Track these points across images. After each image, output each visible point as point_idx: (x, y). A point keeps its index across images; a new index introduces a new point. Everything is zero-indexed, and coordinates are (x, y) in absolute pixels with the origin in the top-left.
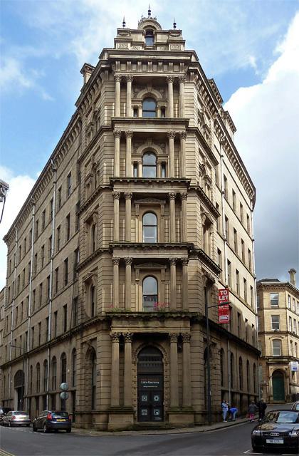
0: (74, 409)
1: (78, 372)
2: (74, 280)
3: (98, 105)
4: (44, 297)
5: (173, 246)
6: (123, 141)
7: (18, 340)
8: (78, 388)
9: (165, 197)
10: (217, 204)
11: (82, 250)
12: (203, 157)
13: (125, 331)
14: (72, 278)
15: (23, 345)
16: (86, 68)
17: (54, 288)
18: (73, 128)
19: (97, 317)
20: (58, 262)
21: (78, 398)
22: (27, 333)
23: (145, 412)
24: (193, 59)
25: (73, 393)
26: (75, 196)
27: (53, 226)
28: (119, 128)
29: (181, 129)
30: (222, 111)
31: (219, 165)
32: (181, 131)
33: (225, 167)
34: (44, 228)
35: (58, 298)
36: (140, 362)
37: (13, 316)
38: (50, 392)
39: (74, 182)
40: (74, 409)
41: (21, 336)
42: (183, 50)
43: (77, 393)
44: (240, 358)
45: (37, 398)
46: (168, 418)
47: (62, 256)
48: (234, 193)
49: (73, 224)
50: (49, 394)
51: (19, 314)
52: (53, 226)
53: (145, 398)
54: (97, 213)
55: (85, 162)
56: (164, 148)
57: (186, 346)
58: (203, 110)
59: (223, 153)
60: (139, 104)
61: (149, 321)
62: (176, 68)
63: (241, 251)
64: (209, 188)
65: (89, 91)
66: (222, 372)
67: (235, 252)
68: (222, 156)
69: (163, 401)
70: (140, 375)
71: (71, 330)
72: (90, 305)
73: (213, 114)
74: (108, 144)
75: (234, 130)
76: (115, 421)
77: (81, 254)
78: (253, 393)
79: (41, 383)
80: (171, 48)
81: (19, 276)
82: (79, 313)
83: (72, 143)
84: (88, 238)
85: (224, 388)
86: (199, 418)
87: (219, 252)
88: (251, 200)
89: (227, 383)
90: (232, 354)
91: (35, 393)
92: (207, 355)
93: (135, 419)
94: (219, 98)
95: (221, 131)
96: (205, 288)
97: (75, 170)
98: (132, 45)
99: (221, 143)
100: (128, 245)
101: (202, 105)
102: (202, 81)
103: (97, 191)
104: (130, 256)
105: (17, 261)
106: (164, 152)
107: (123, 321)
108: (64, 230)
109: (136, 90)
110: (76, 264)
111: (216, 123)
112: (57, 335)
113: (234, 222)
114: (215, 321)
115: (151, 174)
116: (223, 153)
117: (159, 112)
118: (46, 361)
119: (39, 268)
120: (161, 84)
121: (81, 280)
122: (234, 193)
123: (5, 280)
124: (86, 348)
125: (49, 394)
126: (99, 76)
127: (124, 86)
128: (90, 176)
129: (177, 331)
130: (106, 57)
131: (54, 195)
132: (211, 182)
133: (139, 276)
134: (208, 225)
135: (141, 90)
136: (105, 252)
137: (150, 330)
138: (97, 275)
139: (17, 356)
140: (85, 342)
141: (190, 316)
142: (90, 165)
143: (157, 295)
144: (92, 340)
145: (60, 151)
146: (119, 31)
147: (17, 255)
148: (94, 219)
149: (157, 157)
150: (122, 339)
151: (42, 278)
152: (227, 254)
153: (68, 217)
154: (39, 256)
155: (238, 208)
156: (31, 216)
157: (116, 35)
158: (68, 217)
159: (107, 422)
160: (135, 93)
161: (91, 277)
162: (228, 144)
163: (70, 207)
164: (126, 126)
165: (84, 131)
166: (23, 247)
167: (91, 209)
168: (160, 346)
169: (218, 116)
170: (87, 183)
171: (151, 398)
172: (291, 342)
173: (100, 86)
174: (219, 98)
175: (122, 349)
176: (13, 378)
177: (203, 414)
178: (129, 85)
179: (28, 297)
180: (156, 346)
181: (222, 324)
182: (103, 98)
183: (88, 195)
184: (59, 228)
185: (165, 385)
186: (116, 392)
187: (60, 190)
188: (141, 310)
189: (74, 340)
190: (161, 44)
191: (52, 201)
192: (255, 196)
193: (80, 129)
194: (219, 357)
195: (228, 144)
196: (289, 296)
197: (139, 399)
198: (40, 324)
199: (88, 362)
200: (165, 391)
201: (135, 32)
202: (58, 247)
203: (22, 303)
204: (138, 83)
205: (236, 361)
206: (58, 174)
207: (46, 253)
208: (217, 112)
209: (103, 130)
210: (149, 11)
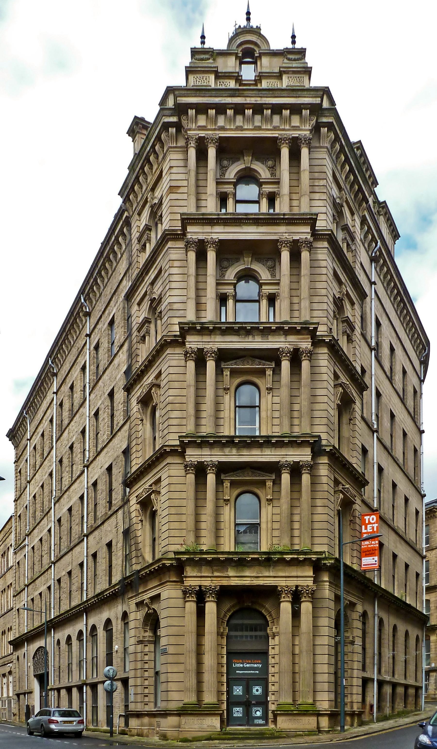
0: (127, 706)
1: (131, 649)
3: (158, 193)
4: (76, 529)
5: (286, 440)
6: (201, 258)
8: (131, 674)
9: (273, 356)
10: (362, 367)
11: (134, 450)
12: (340, 283)
13: (206, 583)
16: (137, 126)
18: (117, 239)
19: (160, 560)
20: (97, 471)
21: (131, 690)
22: (49, 588)
24: (326, 104)
25: (125, 682)
26: (123, 357)
28: (195, 232)
29: (303, 232)
31: (368, 299)
32: (303, 237)
33: (377, 303)
36: (233, 633)
38: (88, 682)
39: (119, 334)
40: (127, 706)
41: (40, 594)
42: (307, 86)
43: (131, 682)
45: (69, 690)
47: (104, 461)
48: (392, 350)
49: (119, 408)
50: (87, 685)
53: (238, 690)
54: (159, 386)
56: (272, 269)
57: (306, 607)
58: (340, 198)
61: (245, 566)
62: (296, 121)
64: (350, 340)
65: (142, 168)
66: (364, 649)
68: (374, 283)
71: (124, 579)
72: (148, 541)
73: (360, 205)
74: (176, 264)
75: (396, 236)
79: (75, 667)
80: (286, 82)
81: (34, 497)
83: (115, 264)
85: (366, 675)
86: (325, 722)
88: (421, 363)
90: (381, 622)
91: (65, 683)
96: (339, 511)
99: (373, 260)
101: (340, 188)
102: (341, 146)
104: (215, 459)
105: (29, 472)
106: (273, 275)
107: (203, 568)
108: (104, 416)
109: (225, 163)
111: (364, 221)
112: (98, 591)
113: (391, 401)
114: (355, 567)
115: (246, 314)
117: (264, 202)
118: (81, 633)
119: (66, 482)
120: (266, 149)
121: (133, 500)
122: (392, 350)
125: (87, 685)
126: (159, 138)
127: (202, 156)
128: (147, 321)
129: (292, 583)
130: (170, 103)
132: (352, 329)
134: (345, 404)
135: (233, 163)
136: (173, 452)
137: (247, 582)
138: (159, 493)
139: (37, 624)
142: (146, 304)
145: (95, 280)
146: (194, 52)
148: (154, 396)
149: (261, 285)
150: (200, 596)
153: (111, 395)
155: (398, 377)
158: (111, 395)
160: (222, 168)
163: (116, 377)
164: (208, 229)
165: (135, 241)
166: (38, 447)
167: (149, 379)
168: (264, 607)
169: (369, 209)
171: (248, 690)
173: (160, 158)
178: (212, 152)
179: (49, 531)
180: (258, 608)
183: (144, 352)
184: (96, 414)
190: (269, 76)
193: (128, 237)
194: (359, 625)
195: (385, 261)
197: (229, 692)
198: (70, 573)
199: (147, 634)
201: (222, 54)
203: (41, 540)
204: (229, 149)
205: (388, 630)
206: (94, 320)
207: (78, 458)
208: (367, 202)
209: (169, 236)
210: (248, 13)
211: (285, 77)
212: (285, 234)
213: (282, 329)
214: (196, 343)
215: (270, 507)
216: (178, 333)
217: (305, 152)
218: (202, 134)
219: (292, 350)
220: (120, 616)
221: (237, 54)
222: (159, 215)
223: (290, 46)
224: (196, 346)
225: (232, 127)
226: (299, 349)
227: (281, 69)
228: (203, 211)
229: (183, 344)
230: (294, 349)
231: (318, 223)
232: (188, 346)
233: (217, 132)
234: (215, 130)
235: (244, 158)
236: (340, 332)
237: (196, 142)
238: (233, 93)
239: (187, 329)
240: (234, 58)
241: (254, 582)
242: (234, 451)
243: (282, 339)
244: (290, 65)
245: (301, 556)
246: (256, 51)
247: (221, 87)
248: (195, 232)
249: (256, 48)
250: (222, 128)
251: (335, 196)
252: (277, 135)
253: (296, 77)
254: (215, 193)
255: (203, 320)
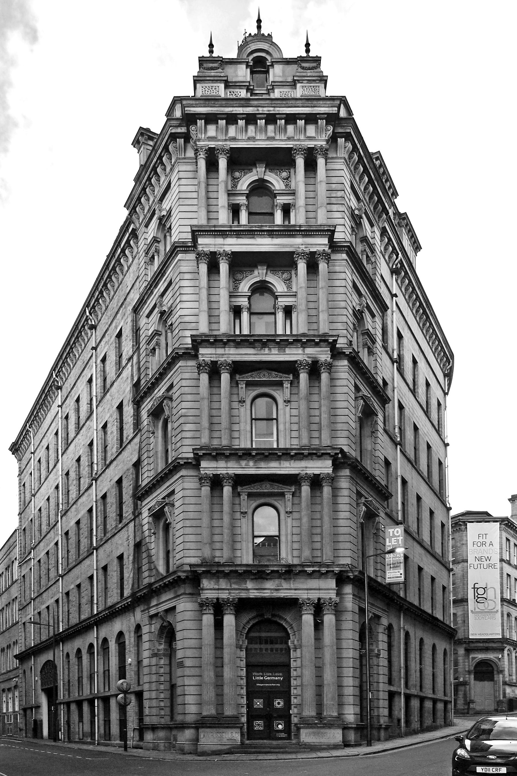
1: (146, 662)
2: (134, 513)
3: (166, 205)
4: (84, 542)
7: (44, 614)
12: (360, 294)
13: (224, 595)
14: (131, 510)
15: (51, 623)
17: (101, 527)
19: (175, 572)
20: (106, 484)
22: (57, 601)
23: (259, 725)
25: (139, 695)
27: (94, 424)
28: (206, 243)
29: (320, 243)
30: (397, 213)
31: (389, 312)
32: (321, 249)
33: (400, 316)
34: (79, 428)
35: (106, 546)
36: (251, 646)
37: (33, 578)
39: (127, 348)
42: (323, 96)
43: (146, 695)
44: (422, 641)
45: (79, 704)
46: (297, 736)
51: (43, 572)
52: (94, 424)
53: (258, 703)
54: (171, 399)
55: (146, 310)
56: (288, 281)
59: (395, 290)
60: (242, 200)
62: (311, 130)
63: (426, 464)
64: (371, 352)
65: (149, 179)
67: (414, 464)
68: (396, 296)
69: (290, 708)
70: (250, 667)
73: (380, 217)
74: (187, 276)
75: (417, 247)
76: (210, 739)
77: (145, 469)
78: (443, 698)
81: (40, 510)
82: (145, 568)
84: (156, 442)
85: (392, 689)
86: (352, 736)
87: (387, 463)
88: (445, 375)
89: (397, 680)
90: (407, 634)
91: (75, 695)
92: (364, 635)
93: (242, 735)
94: (390, 188)
95: (394, 249)
96: (362, 524)
97: (130, 324)
98: (227, 87)
100: (227, 453)
103: (169, 360)
104: (231, 472)
106: (289, 287)
110: (136, 486)
111: (384, 232)
112: (109, 604)
114: (379, 579)
116: (395, 290)
118: (91, 646)
119: (73, 495)
120: (280, 159)
121: (145, 513)
122: (415, 362)
123: (18, 517)
124: (156, 626)
125: (98, 698)
126: (166, 148)
128: (157, 333)
129: (314, 596)
130: (178, 113)
131: (93, 370)
132: (374, 342)
133: (246, 504)
134: (367, 415)
136: (187, 465)
137: (267, 594)
138: (173, 505)
139: (44, 638)
140: (156, 615)
141: (337, 569)
142: (156, 315)
143: (279, 536)
144: (167, 611)
146: (202, 61)
147: (36, 475)
148: (166, 409)
150: (218, 608)
151: (79, 512)
152: (400, 466)
153: (120, 407)
154: (73, 475)
156: (54, 409)
157: (195, 69)
158: (120, 407)
159: (197, 740)
161: (164, 507)
162: (405, 271)
163: (123, 390)
164: (220, 241)
166: (43, 461)
167: (160, 391)
170: (151, 346)
171: (268, 703)
172: (509, 615)
173: (168, 169)
174: (387, 181)
175: (219, 625)
176: (39, 673)
177: (359, 729)
179: (57, 544)
181: (390, 584)
182: (174, 190)
184: (105, 427)
185: (293, 682)
186: (210, 694)
187: (104, 360)
188: (251, 562)
189: (138, 612)
190: (282, 84)
191: (90, 381)
192: (452, 369)
195: (406, 273)
196: (508, 540)
197: (250, 705)
198: (79, 586)
200: (293, 691)
201: (231, 62)
202: (105, 460)
203: (47, 553)
205: (414, 644)
208: (387, 213)
209: (177, 248)
210: (259, 21)
211: (298, 85)
212: (301, 247)
213: (300, 341)
214: (210, 356)
215: (289, 520)
216: (190, 346)
217: (321, 162)
218: (212, 144)
219: (310, 362)
220: (133, 629)
221: (248, 62)
222: (168, 227)
223: (305, 55)
224: (210, 358)
225: (244, 138)
226: (318, 361)
227: (295, 79)
228: (213, 223)
229: (195, 356)
230: (312, 361)
231: (336, 235)
232: (201, 358)
233: (228, 143)
234: (226, 140)
235: (256, 168)
236: (361, 344)
237: (206, 153)
238: (245, 102)
239: (199, 342)
240: (244, 66)
241: (274, 594)
242: (251, 464)
243: (300, 351)
244: (304, 74)
245: (323, 569)
246: (268, 60)
247: (231, 97)
248: (206, 243)
249: (268, 57)
250: (234, 139)
251: (353, 208)
252: (292, 146)
253: (311, 86)
254: (226, 206)
255: (215, 333)
